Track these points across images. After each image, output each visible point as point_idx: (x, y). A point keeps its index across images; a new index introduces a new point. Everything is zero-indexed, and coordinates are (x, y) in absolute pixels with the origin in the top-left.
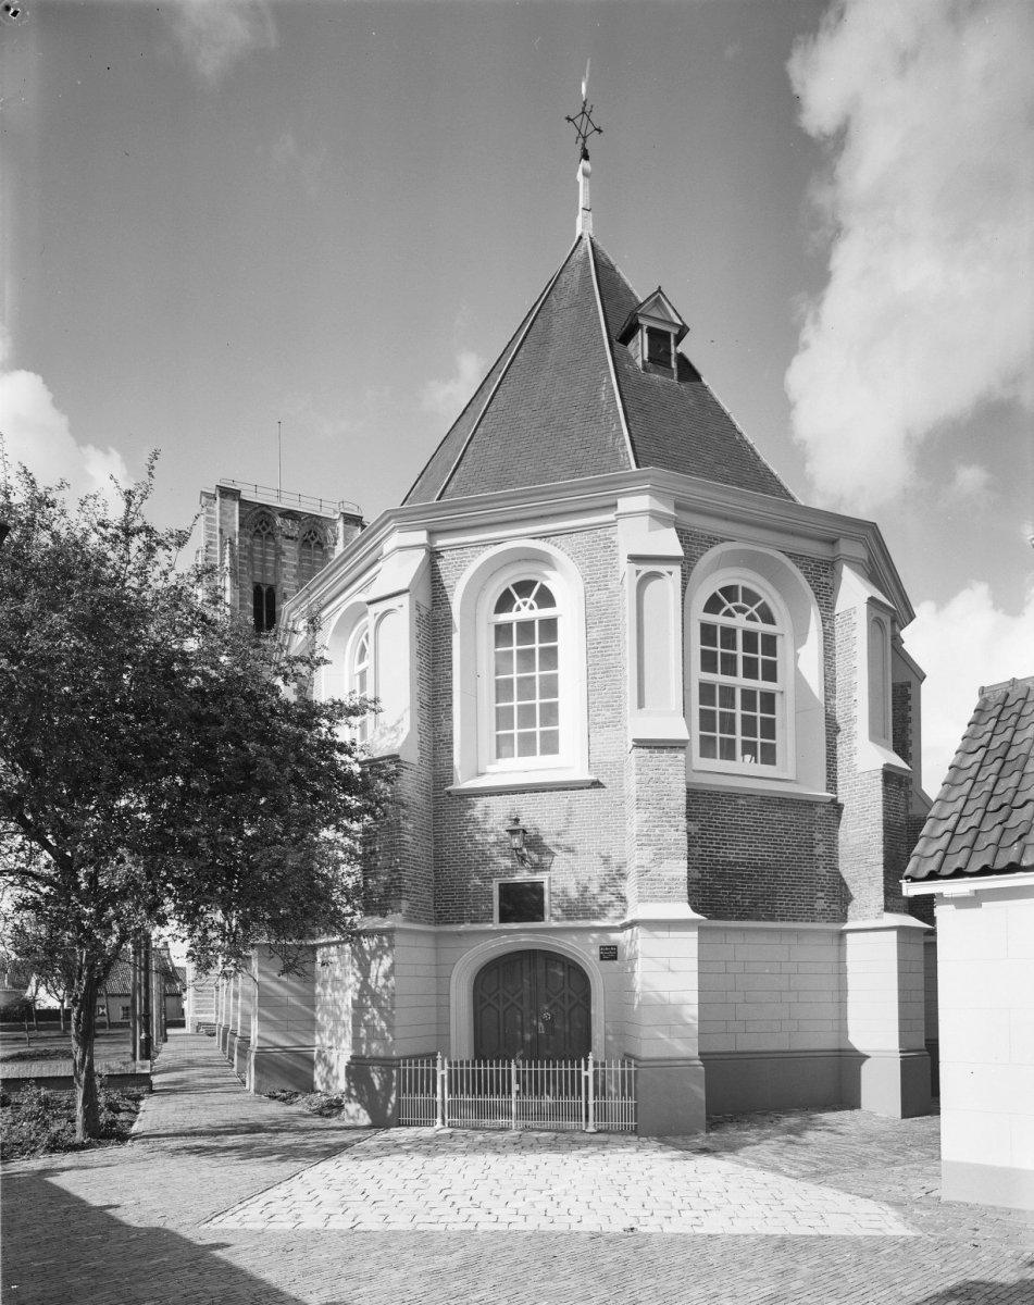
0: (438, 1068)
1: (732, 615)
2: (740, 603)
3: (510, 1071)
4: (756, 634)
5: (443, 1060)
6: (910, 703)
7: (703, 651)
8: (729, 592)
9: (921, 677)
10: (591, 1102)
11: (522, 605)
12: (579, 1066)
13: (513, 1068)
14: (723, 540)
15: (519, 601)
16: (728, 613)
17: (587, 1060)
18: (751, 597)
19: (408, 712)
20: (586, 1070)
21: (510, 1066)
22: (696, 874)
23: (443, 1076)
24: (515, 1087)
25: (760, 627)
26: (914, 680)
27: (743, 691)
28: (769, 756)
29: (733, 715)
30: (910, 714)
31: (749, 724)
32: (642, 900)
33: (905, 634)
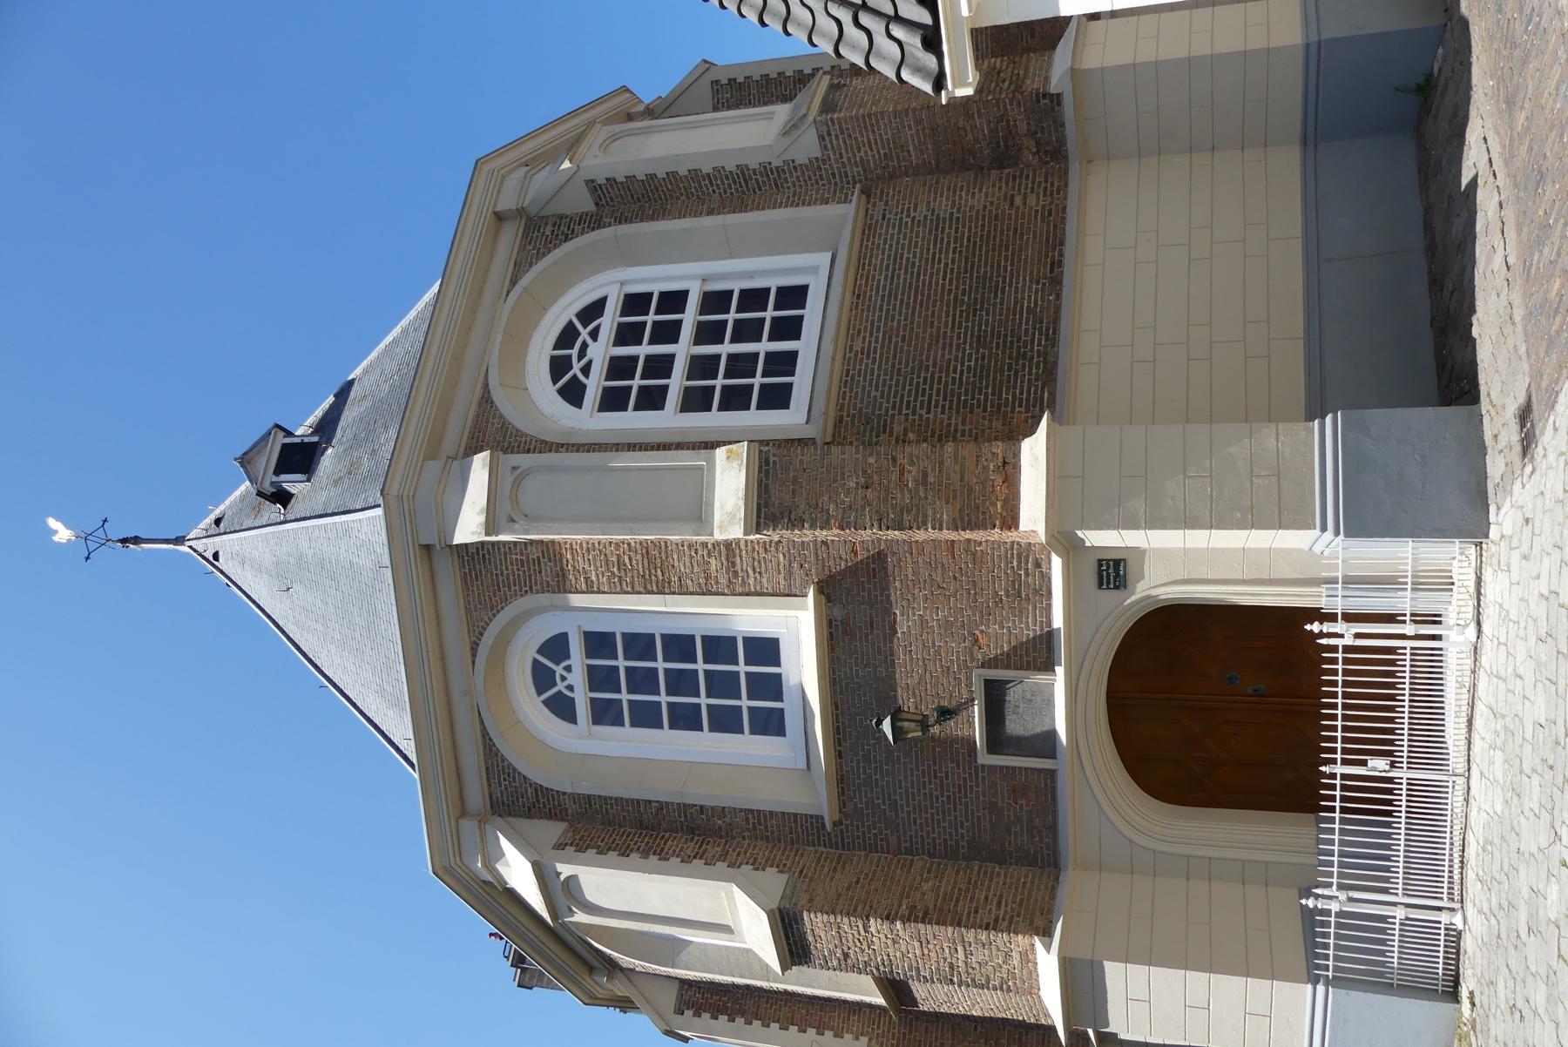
1: (590, 363)
2: (574, 352)
3: (1344, 777)
4: (699, 323)
5: (1317, 896)
6: (773, 75)
7: (722, 408)
8: (559, 367)
9: (708, 65)
10: (1400, 913)
12: (1334, 649)
13: (1339, 769)
14: (486, 385)
15: (561, 686)
16: (586, 370)
17: (1322, 635)
18: (567, 336)
20: (1342, 636)
21: (1333, 776)
22: (1020, 413)
24: (1378, 765)
25: (609, 321)
26: (711, 76)
27: (696, 343)
28: (794, 296)
29: (769, 355)
31: (747, 331)
32: (1011, 520)
33: (648, 98)
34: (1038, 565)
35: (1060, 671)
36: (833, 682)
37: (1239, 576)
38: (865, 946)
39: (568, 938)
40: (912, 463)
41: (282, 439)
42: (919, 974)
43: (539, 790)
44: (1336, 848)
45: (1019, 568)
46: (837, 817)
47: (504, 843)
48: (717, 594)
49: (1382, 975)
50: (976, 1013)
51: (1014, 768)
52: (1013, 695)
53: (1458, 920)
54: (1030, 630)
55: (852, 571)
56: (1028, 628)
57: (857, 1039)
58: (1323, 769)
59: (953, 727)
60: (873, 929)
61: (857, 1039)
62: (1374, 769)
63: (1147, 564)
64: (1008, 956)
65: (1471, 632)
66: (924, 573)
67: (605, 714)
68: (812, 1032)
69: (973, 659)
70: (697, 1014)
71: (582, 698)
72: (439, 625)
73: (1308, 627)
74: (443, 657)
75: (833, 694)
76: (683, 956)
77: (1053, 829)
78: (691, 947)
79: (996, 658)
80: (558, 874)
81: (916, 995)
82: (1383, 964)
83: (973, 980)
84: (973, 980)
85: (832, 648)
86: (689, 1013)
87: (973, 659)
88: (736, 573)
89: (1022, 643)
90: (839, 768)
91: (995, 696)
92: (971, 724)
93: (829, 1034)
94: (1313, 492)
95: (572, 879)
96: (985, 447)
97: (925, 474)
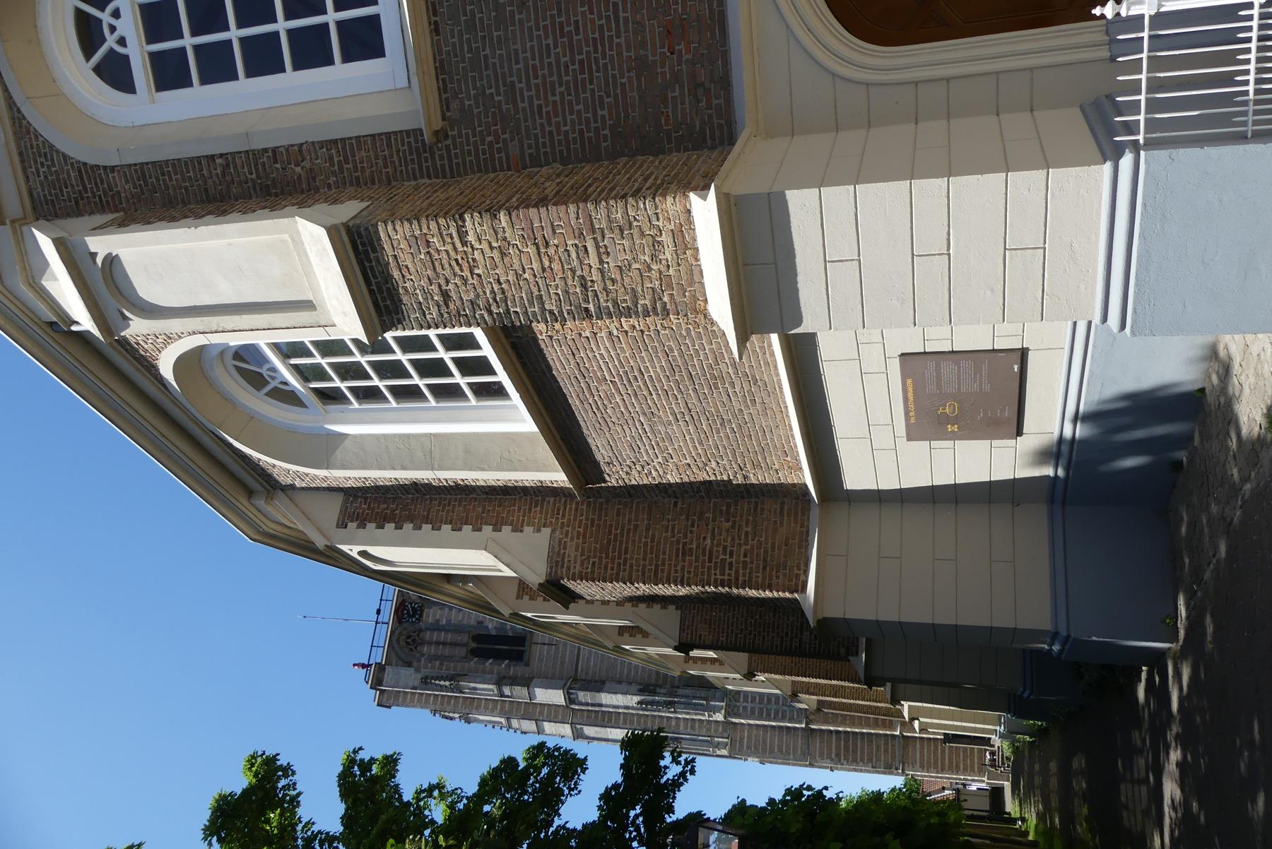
11: (116, 35)
38: (466, 273)
39: (196, 431)
42: (543, 309)
43: (86, 171)
46: (438, 124)
47: (36, 232)
49: (1226, 120)
50: (673, 478)
57: (539, 531)
60: (471, 238)
61: (539, 531)
64: (656, 244)
67: (170, 73)
68: (487, 529)
70: (362, 525)
71: (138, 54)
76: (339, 454)
77: (725, 82)
78: (347, 442)
81: (598, 457)
82: (1227, 99)
83: (615, 303)
84: (615, 303)
86: (352, 526)
90: (437, 50)
93: (507, 529)
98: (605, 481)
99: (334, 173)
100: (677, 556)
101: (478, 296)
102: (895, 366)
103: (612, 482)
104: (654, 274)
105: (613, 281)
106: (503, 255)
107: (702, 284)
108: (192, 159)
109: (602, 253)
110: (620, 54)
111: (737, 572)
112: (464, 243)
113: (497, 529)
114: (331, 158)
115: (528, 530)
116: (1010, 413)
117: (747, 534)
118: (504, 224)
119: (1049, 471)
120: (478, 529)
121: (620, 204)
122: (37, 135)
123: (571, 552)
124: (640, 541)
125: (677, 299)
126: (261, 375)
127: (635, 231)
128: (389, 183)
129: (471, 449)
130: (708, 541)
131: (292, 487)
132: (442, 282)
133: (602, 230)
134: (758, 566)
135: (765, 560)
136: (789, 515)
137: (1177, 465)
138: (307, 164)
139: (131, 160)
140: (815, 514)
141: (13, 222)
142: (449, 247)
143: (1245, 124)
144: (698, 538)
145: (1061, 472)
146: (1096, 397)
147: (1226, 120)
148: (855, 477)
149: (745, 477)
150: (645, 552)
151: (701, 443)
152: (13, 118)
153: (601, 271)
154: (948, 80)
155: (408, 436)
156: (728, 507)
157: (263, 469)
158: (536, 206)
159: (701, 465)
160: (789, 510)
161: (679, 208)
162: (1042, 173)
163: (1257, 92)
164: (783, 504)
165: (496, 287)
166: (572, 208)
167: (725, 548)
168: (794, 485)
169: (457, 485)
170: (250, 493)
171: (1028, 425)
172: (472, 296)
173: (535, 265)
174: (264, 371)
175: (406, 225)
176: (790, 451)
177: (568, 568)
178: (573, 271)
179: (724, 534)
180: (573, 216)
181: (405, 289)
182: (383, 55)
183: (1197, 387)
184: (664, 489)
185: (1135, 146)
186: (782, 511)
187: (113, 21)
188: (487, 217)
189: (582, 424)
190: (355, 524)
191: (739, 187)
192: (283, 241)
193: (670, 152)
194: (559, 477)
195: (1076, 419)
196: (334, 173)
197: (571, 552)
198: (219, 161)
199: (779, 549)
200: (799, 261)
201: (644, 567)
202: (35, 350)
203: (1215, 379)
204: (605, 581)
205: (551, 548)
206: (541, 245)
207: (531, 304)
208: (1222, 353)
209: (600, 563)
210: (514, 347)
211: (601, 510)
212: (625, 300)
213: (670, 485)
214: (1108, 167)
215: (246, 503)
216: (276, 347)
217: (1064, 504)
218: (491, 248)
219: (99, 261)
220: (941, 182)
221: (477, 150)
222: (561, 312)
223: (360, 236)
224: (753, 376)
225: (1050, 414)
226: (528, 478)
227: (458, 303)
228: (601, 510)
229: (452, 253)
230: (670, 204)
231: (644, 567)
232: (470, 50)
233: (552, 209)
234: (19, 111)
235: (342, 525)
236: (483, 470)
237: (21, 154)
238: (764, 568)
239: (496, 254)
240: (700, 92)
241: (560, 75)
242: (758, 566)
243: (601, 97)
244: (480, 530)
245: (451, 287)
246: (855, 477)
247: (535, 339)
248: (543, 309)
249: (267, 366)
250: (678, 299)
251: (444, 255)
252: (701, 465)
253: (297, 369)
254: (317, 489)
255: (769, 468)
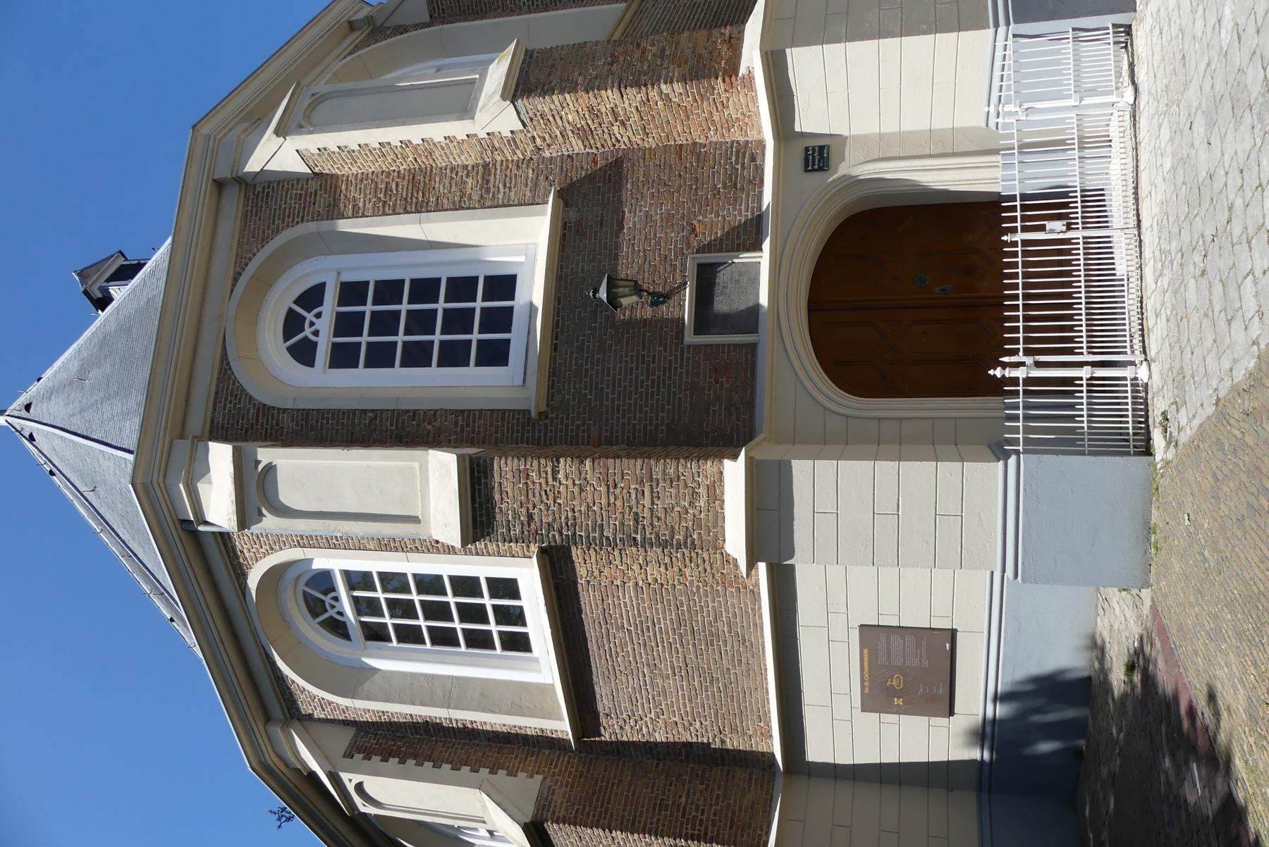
0: (1020, 373)
3: (1026, 243)
5: (1004, 365)
8: (293, 324)
10: (1085, 373)
11: (313, 329)
13: (1019, 237)
19: (480, 104)
21: (1015, 244)
23: (1039, 365)
24: (1055, 229)
30: (394, 761)
34: (753, 159)
35: (766, 245)
36: (559, 279)
37: (927, 152)
40: (653, 45)
41: (121, 261)
42: (602, 535)
44: (1020, 324)
45: (737, 163)
46: (543, 408)
48: (469, 208)
50: (659, 737)
51: (717, 346)
52: (723, 277)
53: (1143, 374)
54: (741, 215)
55: (590, 178)
56: (740, 214)
57: (531, 777)
58: (1005, 238)
59: (665, 310)
60: (561, 476)
61: (531, 777)
62: (1052, 231)
63: (847, 148)
64: (695, 495)
65: (1129, 93)
66: (654, 175)
67: (343, 357)
68: (484, 772)
69: (689, 246)
70: (368, 757)
72: (210, 258)
73: (991, 372)
74: (205, 287)
75: (558, 290)
76: (367, 686)
77: (751, 405)
79: (710, 243)
80: (258, 462)
82: (1072, 431)
83: (657, 536)
84: (657, 536)
85: (563, 247)
86: (358, 757)
87: (689, 246)
88: (488, 190)
89: (734, 228)
90: (553, 360)
91: (706, 279)
92: (682, 307)
93: (502, 773)
94: (987, 9)
95: (270, 468)
96: (715, 32)
97: (663, 50)
98: (600, 735)
99: (456, 433)
100: (654, 810)
101: (554, 520)
102: (855, 635)
103: (606, 736)
104: (690, 516)
105: (659, 519)
106: (581, 490)
107: (723, 527)
108: (349, 411)
109: (655, 497)
110: (681, 379)
111: (706, 829)
112: (555, 479)
113: (493, 771)
114: (457, 422)
115: (522, 775)
116: (943, 690)
117: (718, 796)
118: (587, 468)
119: (975, 754)
120: (475, 770)
121: (674, 463)
122: (236, 381)
123: (558, 798)
124: (622, 794)
125: (700, 540)
126: (323, 602)
127: (681, 483)
128: (496, 444)
129: (487, 695)
130: (683, 800)
131: (310, 717)
132: (530, 506)
133: (658, 480)
134: (725, 825)
135: (732, 820)
136: (756, 783)
137: (1078, 754)
138: (437, 424)
139: (301, 406)
140: (779, 782)
141: (194, 437)
142: (543, 481)
143: (1083, 446)
144: (675, 796)
145: (986, 756)
146: (1009, 679)
147: (1072, 442)
148: (816, 752)
149: (723, 742)
150: (626, 805)
151: (690, 701)
152: (221, 369)
153: (651, 510)
154: (900, 419)
155: (433, 677)
156: (704, 773)
157: (291, 694)
158: (614, 458)
159: (686, 724)
160: (757, 779)
161: (715, 469)
162: (959, 464)
163: (1089, 428)
164: (751, 773)
165: (570, 514)
166: (639, 462)
167: (697, 806)
168: (763, 754)
169: (465, 727)
170: (268, 719)
171: (958, 707)
172: (550, 519)
173: (603, 501)
174: (328, 599)
175: (516, 460)
176: (764, 717)
177: (554, 812)
178: (631, 508)
179: (698, 795)
180: (639, 467)
181: (501, 509)
182: (506, 365)
183: (1085, 674)
184: (650, 748)
185: (1017, 453)
186: (750, 778)
187: (314, 320)
188: (576, 461)
189: (594, 670)
190: (361, 756)
191: (760, 455)
192: (411, 468)
193: (707, 445)
194: (562, 726)
195: (996, 699)
196: (456, 433)
197: (558, 798)
198: (369, 414)
199: (746, 812)
200: (918, 45)
201: (623, 816)
202: (161, 541)
203: (1097, 665)
204: (585, 826)
205: (540, 793)
206: (611, 486)
207: (594, 530)
208: (1099, 641)
209: (584, 809)
210: (557, 587)
211: (590, 764)
212: (665, 533)
213: (656, 744)
214: (1001, 463)
215: (261, 725)
216: (347, 574)
217: (990, 792)
218: (574, 484)
219: (260, 467)
220: (895, 464)
221: (567, 427)
222: (615, 539)
223: (478, 465)
224: (743, 636)
225: (975, 699)
226: (530, 724)
227: (538, 524)
228: (590, 764)
229: (544, 485)
230: (709, 466)
231: (623, 816)
232: (576, 364)
233: (625, 461)
234: (228, 363)
235: (349, 755)
236: (494, 712)
237: (216, 393)
238: (731, 827)
239: (576, 490)
240: (733, 409)
241: (636, 388)
242: (725, 825)
243: (663, 405)
244: (477, 771)
245: (536, 511)
246: (816, 752)
247: (576, 583)
248: (602, 535)
249: (333, 594)
250: (704, 537)
251: (538, 486)
252: (686, 724)
253: (356, 601)
254: (333, 721)
255: (744, 734)
